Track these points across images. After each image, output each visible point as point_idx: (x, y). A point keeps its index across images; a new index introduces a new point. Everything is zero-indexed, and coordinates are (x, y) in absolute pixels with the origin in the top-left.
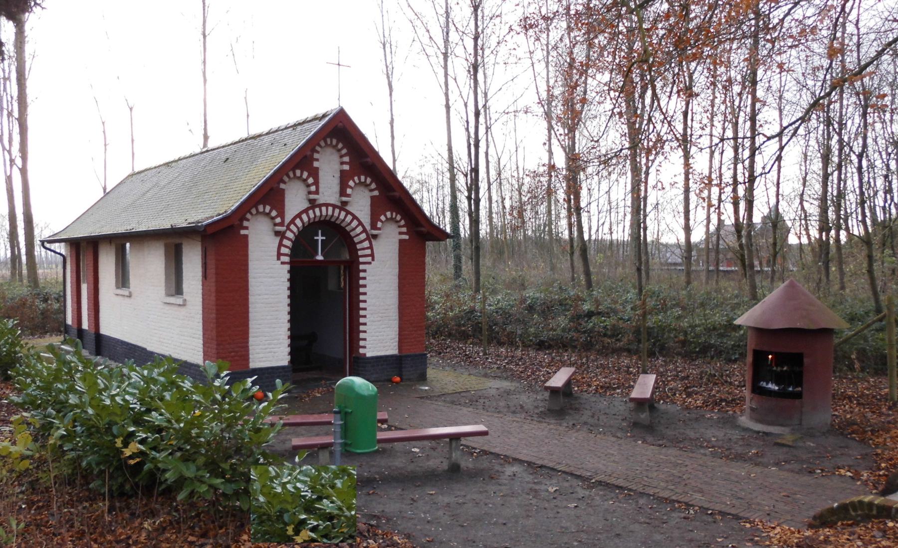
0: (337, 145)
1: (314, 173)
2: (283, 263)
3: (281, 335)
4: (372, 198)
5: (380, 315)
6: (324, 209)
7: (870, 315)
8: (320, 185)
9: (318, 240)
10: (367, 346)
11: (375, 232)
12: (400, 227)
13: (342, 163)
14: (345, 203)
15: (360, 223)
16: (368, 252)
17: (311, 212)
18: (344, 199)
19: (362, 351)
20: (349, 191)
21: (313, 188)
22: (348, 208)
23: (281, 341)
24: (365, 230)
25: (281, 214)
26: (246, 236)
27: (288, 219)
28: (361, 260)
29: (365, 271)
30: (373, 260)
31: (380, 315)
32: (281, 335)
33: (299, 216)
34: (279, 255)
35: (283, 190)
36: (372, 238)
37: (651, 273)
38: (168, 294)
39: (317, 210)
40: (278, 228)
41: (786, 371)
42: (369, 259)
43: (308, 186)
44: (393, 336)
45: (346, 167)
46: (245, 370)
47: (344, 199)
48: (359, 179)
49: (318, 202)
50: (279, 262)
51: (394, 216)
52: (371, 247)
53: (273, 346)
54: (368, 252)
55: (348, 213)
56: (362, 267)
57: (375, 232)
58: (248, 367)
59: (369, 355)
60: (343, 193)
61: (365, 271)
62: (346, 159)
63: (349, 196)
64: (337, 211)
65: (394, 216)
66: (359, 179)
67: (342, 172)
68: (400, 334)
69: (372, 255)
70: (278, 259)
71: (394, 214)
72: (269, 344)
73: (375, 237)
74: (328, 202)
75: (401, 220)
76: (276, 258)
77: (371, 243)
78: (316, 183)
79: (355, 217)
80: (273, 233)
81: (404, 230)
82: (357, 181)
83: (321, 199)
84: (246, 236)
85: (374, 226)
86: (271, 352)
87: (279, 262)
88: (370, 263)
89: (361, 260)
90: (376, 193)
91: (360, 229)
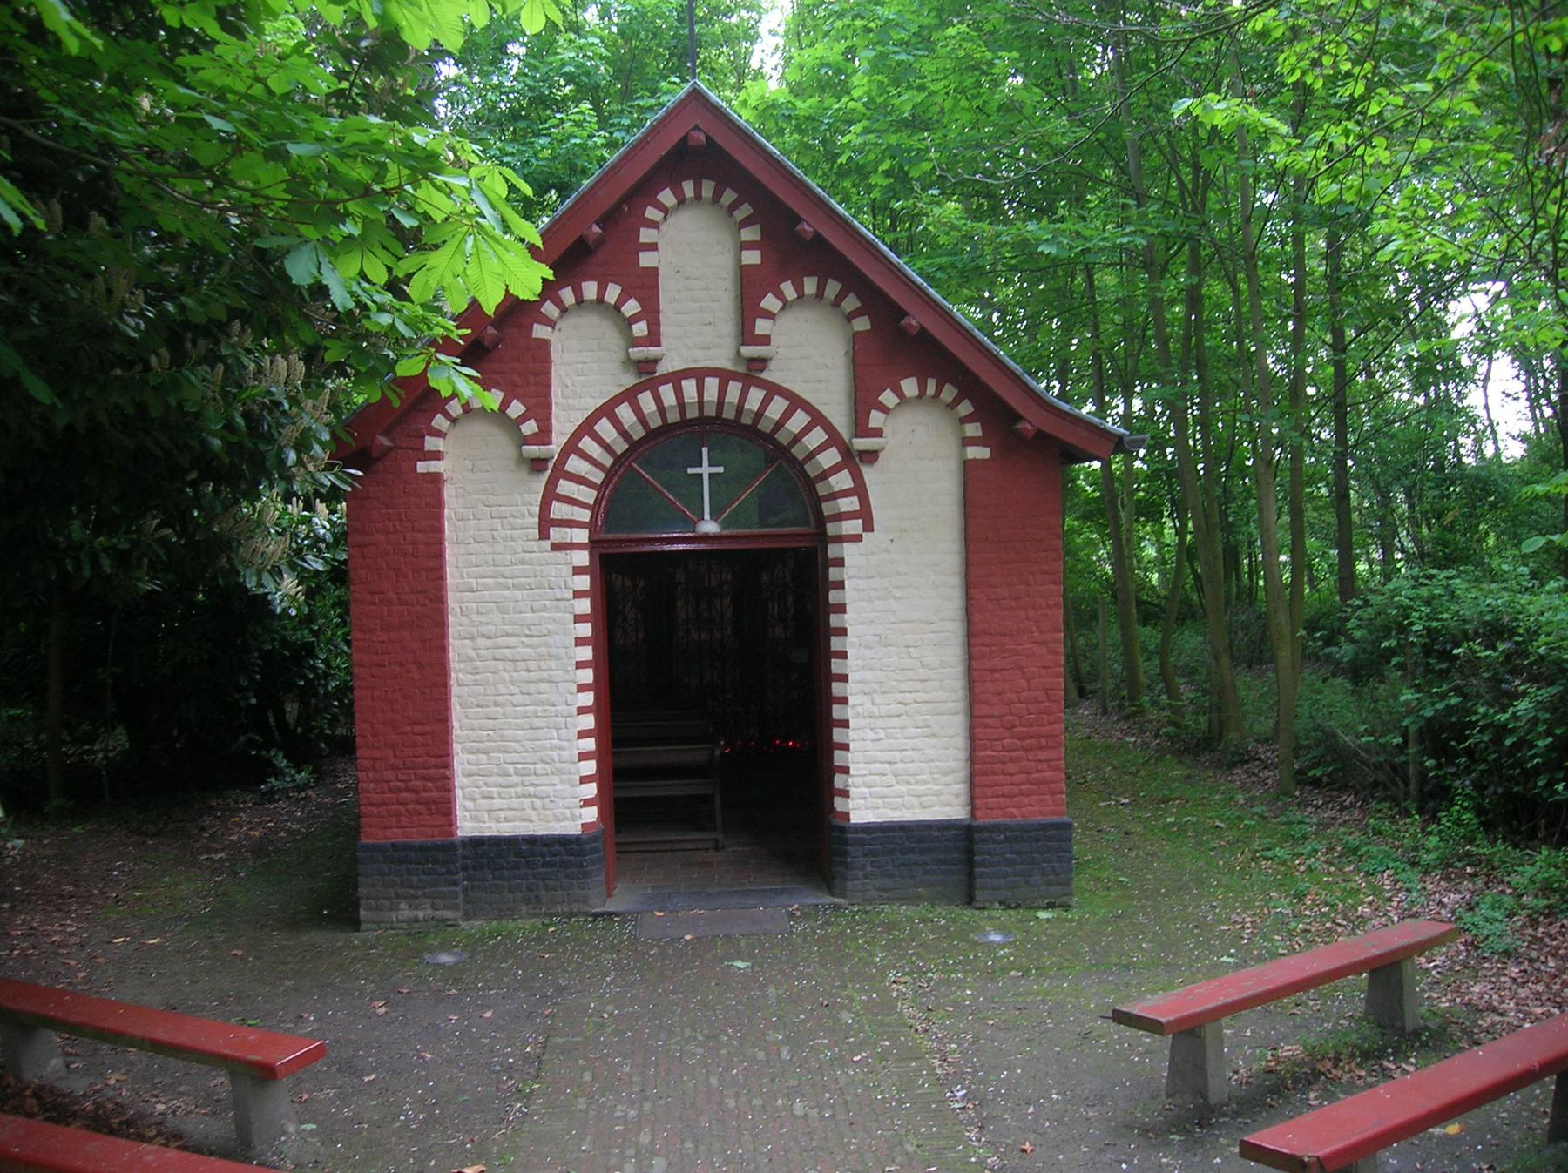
1: (645, 286)
6: (689, 386)
7: (796, 136)
10: (852, 790)
14: (761, 363)
15: (818, 419)
18: (749, 351)
22: (868, 472)
24: (834, 438)
25: (541, 409)
27: (563, 426)
30: (868, 526)
31: (900, 697)
33: (607, 410)
35: (545, 344)
36: (854, 460)
37: (1497, 429)
39: (667, 392)
40: (534, 450)
44: (954, 764)
45: (752, 257)
46: (438, 839)
47: (749, 351)
49: (662, 369)
53: (532, 779)
55: (773, 390)
56: (833, 551)
57: (861, 444)
58: (452, 834)
60: (746, 334)
64: (734, 389)
68: (973, 759)
70: (544, 535)
73: (871, 456)
77: (858, 478)
78: (651, 312)
79: (796, 402)
81: (973, 430)
87: (547, 544)
88: (857, 538)
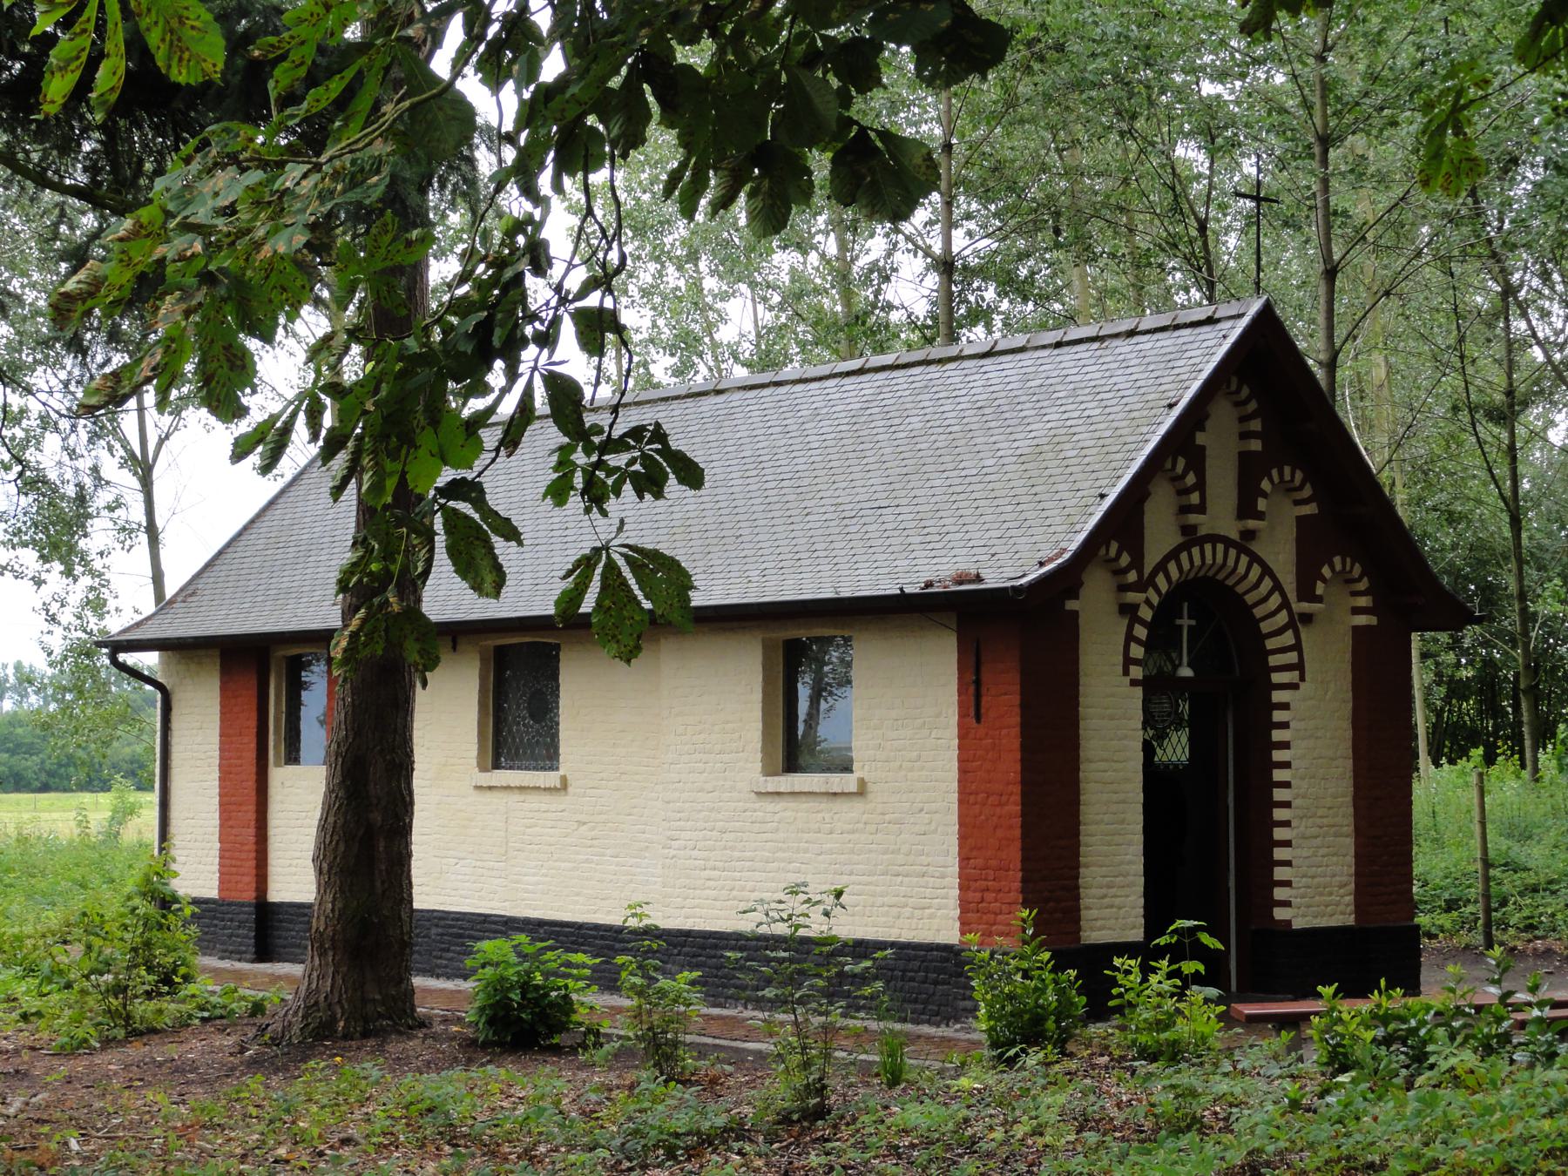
0: (1238, 391)
2: (1134, 683)
3: (1130, 863)
4: (1300, 520)
5: (1319, 821)
8: (1209, 492)
9: (1181, 627)
11: (1305, 607)
12: (1297, 503)
13: (1245, 436)
14: (1249, 535)
16: (1292, 657)
17: (1184, 556)
18: (1252, 524)
19: (1280, 914)
20: (1262, 504)
21: (1195, 498)
22: (1255, 547)
23: (1131, 878)
25: (1137, 562)
26: (1075, 614)
28: (1276, 678)
29: (1285, 706)
30: (1302, 678)
31: (1319, 821)
32: (1130, 863)
34: (1128, 661)
38: (768, 772)
41: (23, 69)
42: (1291, 677)
43: (1187, 491)
45: (1256, 445)
48: (1281, 474)
50: (1127, 680)
51: (1287, 477)
52: (1297, 647)
54: (1292, 657)
55: (1255, 558)
58: (1079, 939)
59: (1298, 924)
61: (1285, 706)
62: (1256, 425)
63: (1260, 516)
65: (1287, 477)
66: (1281, 474)
67: (1245, 458)
69: (1299, 667)
70: (1126, 672)
71: (1287, 470)
72: (1109, 886)
74: (1217, 532)
75: (1359, 580)
76: (1120, 669)
78: (1200, 486)
80: (1116, 608)
82: (1338, 567)
83: (1205, 523)
84: (1075, 614)
85: (1306, 593)
86: (1112, 906)
87: (1127, 680)
89: (1276, 678)
90: (1310, 509)
91: (1275, 600)
